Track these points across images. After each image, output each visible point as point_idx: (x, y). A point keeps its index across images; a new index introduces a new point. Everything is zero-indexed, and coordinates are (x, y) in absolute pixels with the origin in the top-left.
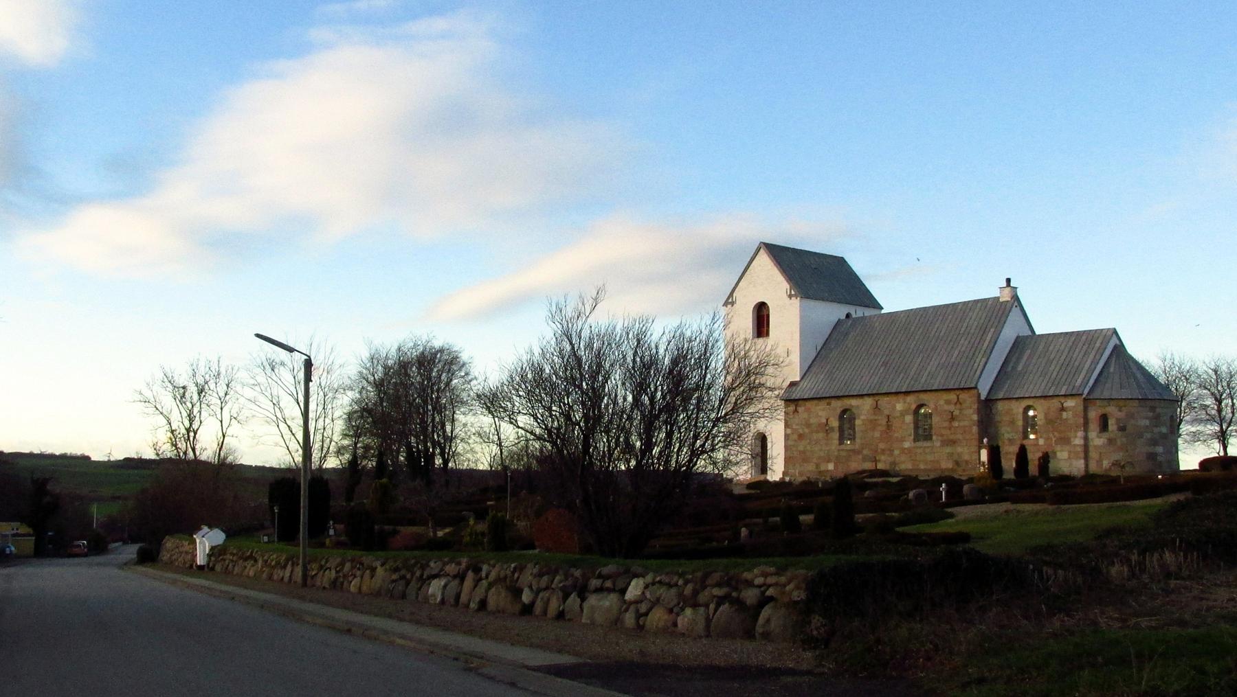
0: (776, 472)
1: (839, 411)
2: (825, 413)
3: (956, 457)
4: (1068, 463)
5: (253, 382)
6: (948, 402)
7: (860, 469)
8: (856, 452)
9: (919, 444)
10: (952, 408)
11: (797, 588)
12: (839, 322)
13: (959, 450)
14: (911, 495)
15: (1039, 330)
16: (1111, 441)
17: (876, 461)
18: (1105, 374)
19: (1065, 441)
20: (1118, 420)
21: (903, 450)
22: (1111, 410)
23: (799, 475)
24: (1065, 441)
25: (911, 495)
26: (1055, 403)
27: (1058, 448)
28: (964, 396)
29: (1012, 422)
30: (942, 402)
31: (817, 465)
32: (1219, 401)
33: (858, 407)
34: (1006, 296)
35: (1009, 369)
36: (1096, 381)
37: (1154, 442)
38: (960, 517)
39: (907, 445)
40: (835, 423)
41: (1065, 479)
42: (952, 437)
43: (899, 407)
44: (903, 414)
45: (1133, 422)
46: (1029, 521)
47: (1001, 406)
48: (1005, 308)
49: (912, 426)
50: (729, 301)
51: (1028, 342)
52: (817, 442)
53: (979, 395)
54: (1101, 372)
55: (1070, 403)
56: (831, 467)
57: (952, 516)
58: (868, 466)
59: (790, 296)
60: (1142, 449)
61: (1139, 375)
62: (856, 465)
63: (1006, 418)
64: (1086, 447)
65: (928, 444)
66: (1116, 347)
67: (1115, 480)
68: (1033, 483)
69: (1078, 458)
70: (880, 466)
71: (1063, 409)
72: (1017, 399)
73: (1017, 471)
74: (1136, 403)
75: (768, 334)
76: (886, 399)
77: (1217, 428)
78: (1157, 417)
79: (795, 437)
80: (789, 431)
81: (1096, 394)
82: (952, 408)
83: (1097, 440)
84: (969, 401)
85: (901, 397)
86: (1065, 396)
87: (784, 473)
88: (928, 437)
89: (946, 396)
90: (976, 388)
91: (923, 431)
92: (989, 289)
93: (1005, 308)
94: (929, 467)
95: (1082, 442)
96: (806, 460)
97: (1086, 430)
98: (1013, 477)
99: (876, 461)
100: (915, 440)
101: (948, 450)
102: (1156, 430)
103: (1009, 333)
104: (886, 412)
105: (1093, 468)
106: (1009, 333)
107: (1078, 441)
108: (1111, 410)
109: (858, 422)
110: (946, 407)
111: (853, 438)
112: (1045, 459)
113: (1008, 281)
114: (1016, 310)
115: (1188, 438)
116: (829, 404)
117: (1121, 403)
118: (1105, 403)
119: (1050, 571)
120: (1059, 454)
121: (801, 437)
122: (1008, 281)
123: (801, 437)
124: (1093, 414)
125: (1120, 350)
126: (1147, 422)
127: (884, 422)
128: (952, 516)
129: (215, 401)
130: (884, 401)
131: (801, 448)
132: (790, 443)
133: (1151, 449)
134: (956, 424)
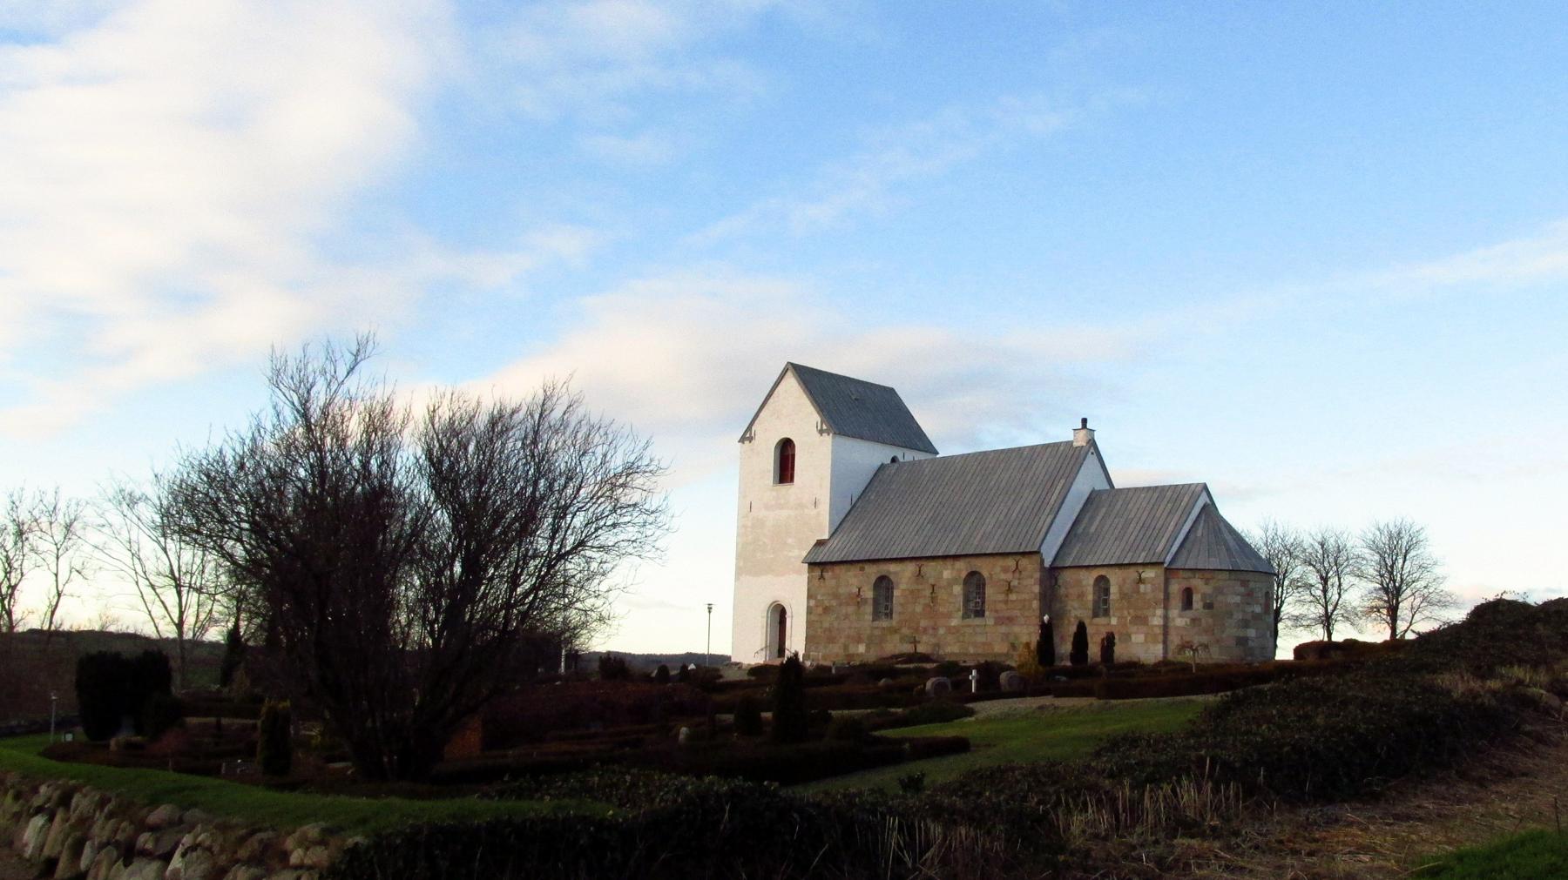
0: (188, 635)
1: (873, 579)
2: (858, 582)
3: (1012, 638)
4: (1141, 647)
5: (102, 522)
6: (1005, 570)
7: (897, 652)
8: (895, 631)
9: (968, 621)
10: (1009, 576)
12: (882, 467)
13: (1016, 629)
14: (929, 684)
15: (1119, 482)
18: (1192, 536)
19: (1141, 620)
20: (1204, 596)
21: (950, 630)
22: (1197, 583)
23: (831, 655)
24: (1141, 620)
25: (929, 684)
26: (1132, 574)
27: (1133, 629)
28: (1024, 562)
29: (1081, 596)
30: (998, 569)
31: (846, 647)
32: (1325, 580)
34: (1080, 440)
35: (1080, 531)
36: (1182, 545)
37: (1245, 624)
38: (981, 716)
39: (954, 622)
40: (869, 594)
41: (1133, 666)
42: (1007, 614)
43: (947, 574)
44: (950, 584)
45: (1220, 598)
46: (1076, 720)
47: (1067, 577)
48: (1080, 454)
49: (961, 599)
50: (747, 437)
51: (1105, 499)
52: (847, 616)
53: (1042, 561)
55: (1149, 574)
56: (862, 649)
57: (971, 713)
58: (907, 648)
59: (821, 432)
60: (1231, 631)
61: (1232, 543)
62: (895, 646)
63: (1074, 591)
64: (1166, 628)
65: (978, 621)
66: (1205, 507)
67: (1185, 668)
68: (1092, 671)
69: (1155, 642)
70: (921, 649)
71: (1140, 581)
72: (1088, 567)
73: (1073, 657)
74: (1226, 575)
75: (792, 480)
76: (933, 564)
77: (1321, 611)
78: (1250, 594)
79: (820, 610)
80: (812, 603)
81: (1178, 565)
82: (1009, 576)
83: (1179, 620)
84: (1030, 567)
85: (949, 563)
86: (1144, 565)
88: (980, 613)
89: (1001, 562)
90: (1038, 552)
91: (975, 604)
92: (1062, 432)
93: (1080, 454)
94: (980, 651)
96: (831, 640)
97: (1166, 608)
98: (1069, 664)
100: (966, 616)
101: (1003, 629)
102: (1249, 609)
103: (1085, 482)
104: (932, 581)
105: (1170, 657)
106: (1085, 482)
107: (1157, 621)
108: (1197, 583)
109: (896, 593)
110: (1003, 576)
111: (889, 615)
112: (1109, 643)
113: (1084, 421)
114: (1091, 460)
115: (1290, 623)
116: (862, 569)
117: (1208, 575)
118: (1189, 574)
119: (936, 830)
120: (1133, 637)
121: (826, 610)
122: (1084, 421)
123: (826, 610)
124: (1176, 588)
125: (1210, 509)
126: (1238, 599)
127: (928, 593)
128: (971, 713)
129: (46, 546)
130: (930, 569)
131: (826, 625)
132: (813, 618)
133: (1241, 633)
134: (1013, 597)
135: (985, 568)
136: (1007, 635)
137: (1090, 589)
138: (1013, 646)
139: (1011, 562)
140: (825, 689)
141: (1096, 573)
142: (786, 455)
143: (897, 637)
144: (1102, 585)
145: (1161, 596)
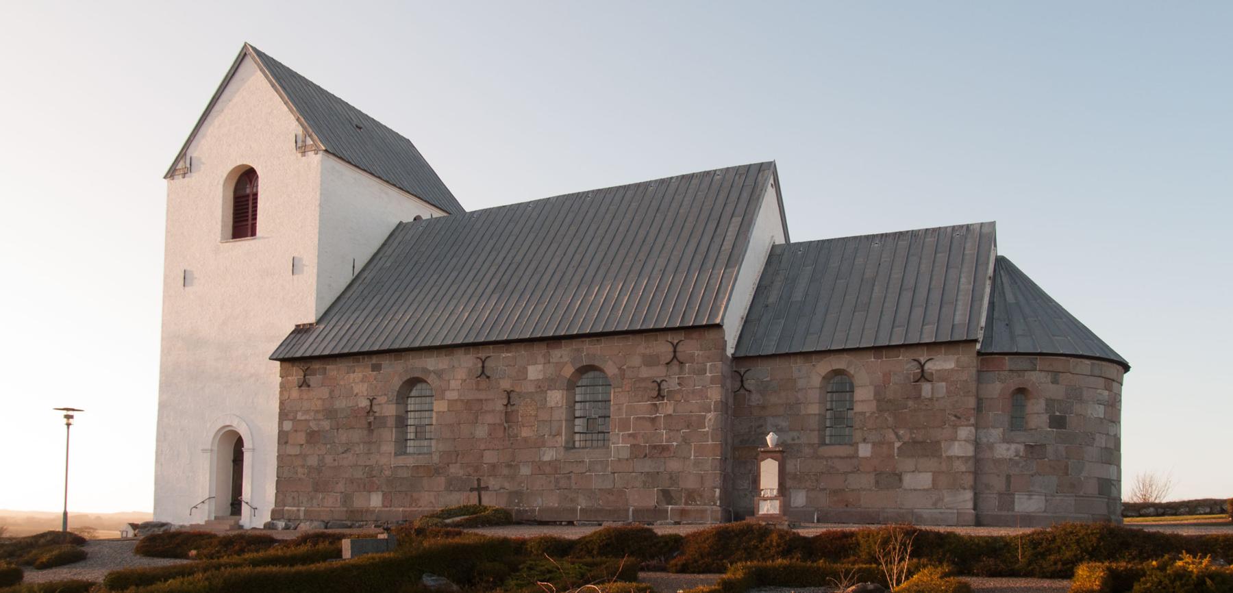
0: (258, 511)
1: (397, 383)
6: (650, 361)
8: (435, 471)
10: (658, 372)
11: (388, 402)
16: (1034, 450)
17: (480, 489)
20: (1050, 403)
21: (539, 467)
23: (356, 560)
24: (925, 448)
26: (904, 365)
27: (909, 464)
28: (691, 347)
30: (636, 361)
31: (347, 498)
33: (439, 374)
43: (535, 372)
44: (544, 386)
50: (180, 167)
54: (992, 304)
55: (942, 363)
56: (376, 501)
64: (978, 463)
69: (955, 486)
71: (923, 376)
72: (806, 355)
75: (253, 234)
76: (506, 355)
79: (301, 438)
80: (288, 426)
82: (658, 372)
85: (539, 351)
87: (276, 514)
89: (643, 347)
95: (970, 451)
96: (320, 487)
99: (480, 489)
101: (648, 466)
104: (506, 384)
110: (645, 372)
116: (376, 368)
117: (1058, 364)
118: (1023, 363)
120: (908, 480)
124: (996, 388)
127: (499, 405)
130: (501, 361)
131: (313, 461)
134: (668, 408)
135: (608, 356)
136: (652, 477)
137: (814, 395)
138: (324, 400)
139: (662, 347)
140: (313, 567)
141: (824, 367)
142: (244, 185)
143: (442, 480)
144: (840, 384)
145: (971, 402)
